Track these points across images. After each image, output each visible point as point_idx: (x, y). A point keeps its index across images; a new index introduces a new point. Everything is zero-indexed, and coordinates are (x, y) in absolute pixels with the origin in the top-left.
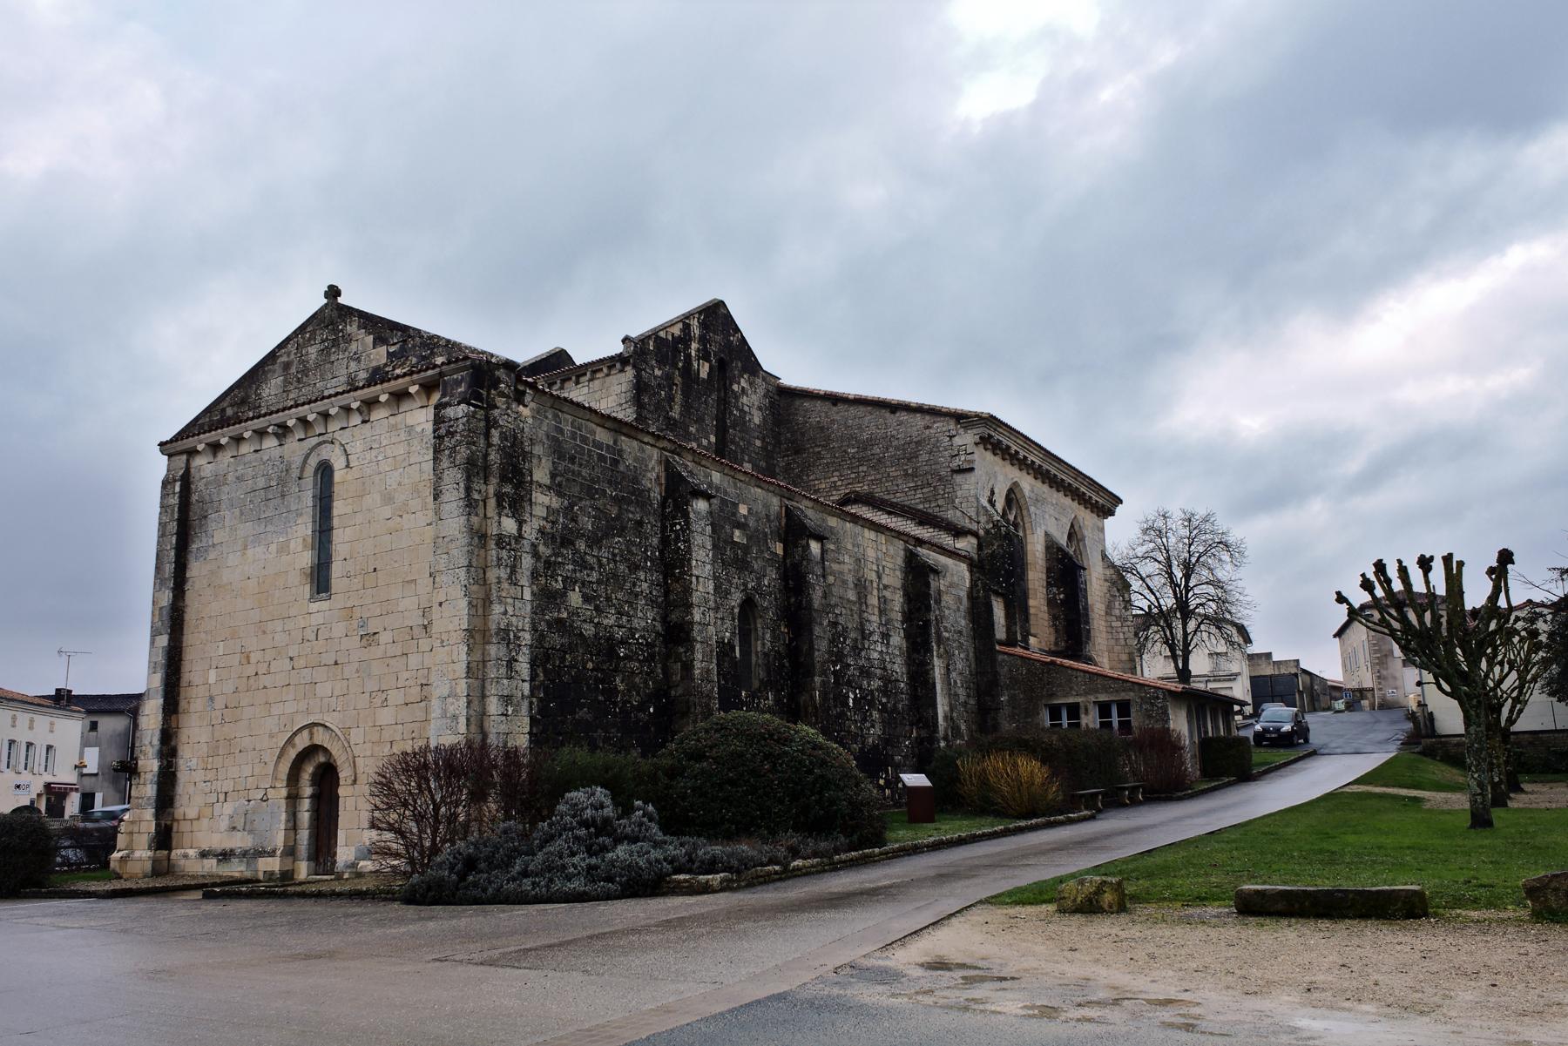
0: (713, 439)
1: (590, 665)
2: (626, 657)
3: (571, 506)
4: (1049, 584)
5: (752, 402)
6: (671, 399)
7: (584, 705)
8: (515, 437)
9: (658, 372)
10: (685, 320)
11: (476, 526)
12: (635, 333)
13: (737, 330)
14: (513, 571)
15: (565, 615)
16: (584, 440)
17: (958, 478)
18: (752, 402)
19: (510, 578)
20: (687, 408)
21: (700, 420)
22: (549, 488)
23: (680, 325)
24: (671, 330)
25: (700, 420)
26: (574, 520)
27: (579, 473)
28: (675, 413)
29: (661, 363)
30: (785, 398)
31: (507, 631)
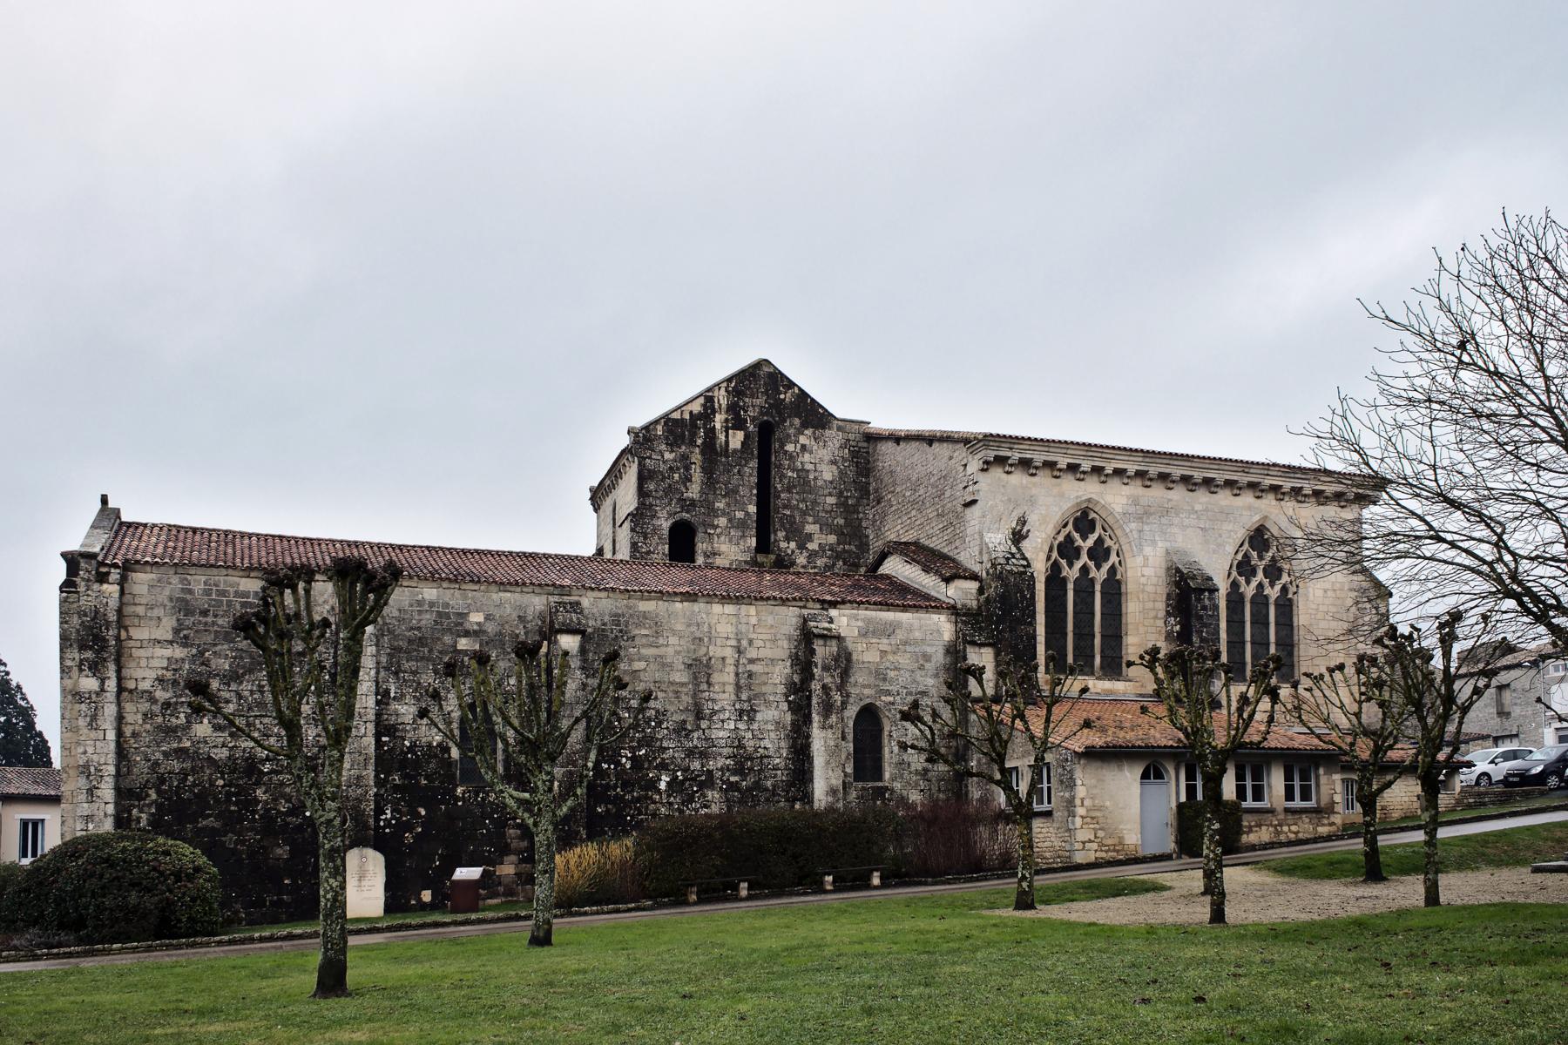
0: (752, 509)
1: (220, 782)
2: (272, 772)
3: (202, 653)
4: (1168, 614)
5: (819, 459)
6: (687, 479)
7: (209, 816)
8: (97, 612)
9: (668, 456)
10: (708, 397)
11: (69, 687)
12: (640, 422)
13: (791, 384)
14: (94, 718)
15: (188, 744)
16: (223, 593)
17: (968, 511)
18: (819, 459)
19: (90, 724)
20: (710, 483)
21: (731, 493)
22: (171, 642)
23: (701, 400)
24: (689, 407)
25: (731, 493)
26: (206, 663)
27: (214, 623)
28: (694, 491)
29: (672, 446)
30: (865, 446)
31: (86, 766)
